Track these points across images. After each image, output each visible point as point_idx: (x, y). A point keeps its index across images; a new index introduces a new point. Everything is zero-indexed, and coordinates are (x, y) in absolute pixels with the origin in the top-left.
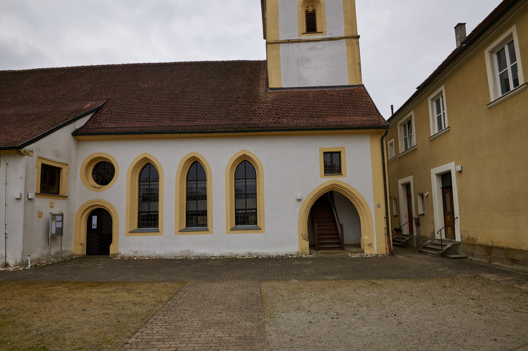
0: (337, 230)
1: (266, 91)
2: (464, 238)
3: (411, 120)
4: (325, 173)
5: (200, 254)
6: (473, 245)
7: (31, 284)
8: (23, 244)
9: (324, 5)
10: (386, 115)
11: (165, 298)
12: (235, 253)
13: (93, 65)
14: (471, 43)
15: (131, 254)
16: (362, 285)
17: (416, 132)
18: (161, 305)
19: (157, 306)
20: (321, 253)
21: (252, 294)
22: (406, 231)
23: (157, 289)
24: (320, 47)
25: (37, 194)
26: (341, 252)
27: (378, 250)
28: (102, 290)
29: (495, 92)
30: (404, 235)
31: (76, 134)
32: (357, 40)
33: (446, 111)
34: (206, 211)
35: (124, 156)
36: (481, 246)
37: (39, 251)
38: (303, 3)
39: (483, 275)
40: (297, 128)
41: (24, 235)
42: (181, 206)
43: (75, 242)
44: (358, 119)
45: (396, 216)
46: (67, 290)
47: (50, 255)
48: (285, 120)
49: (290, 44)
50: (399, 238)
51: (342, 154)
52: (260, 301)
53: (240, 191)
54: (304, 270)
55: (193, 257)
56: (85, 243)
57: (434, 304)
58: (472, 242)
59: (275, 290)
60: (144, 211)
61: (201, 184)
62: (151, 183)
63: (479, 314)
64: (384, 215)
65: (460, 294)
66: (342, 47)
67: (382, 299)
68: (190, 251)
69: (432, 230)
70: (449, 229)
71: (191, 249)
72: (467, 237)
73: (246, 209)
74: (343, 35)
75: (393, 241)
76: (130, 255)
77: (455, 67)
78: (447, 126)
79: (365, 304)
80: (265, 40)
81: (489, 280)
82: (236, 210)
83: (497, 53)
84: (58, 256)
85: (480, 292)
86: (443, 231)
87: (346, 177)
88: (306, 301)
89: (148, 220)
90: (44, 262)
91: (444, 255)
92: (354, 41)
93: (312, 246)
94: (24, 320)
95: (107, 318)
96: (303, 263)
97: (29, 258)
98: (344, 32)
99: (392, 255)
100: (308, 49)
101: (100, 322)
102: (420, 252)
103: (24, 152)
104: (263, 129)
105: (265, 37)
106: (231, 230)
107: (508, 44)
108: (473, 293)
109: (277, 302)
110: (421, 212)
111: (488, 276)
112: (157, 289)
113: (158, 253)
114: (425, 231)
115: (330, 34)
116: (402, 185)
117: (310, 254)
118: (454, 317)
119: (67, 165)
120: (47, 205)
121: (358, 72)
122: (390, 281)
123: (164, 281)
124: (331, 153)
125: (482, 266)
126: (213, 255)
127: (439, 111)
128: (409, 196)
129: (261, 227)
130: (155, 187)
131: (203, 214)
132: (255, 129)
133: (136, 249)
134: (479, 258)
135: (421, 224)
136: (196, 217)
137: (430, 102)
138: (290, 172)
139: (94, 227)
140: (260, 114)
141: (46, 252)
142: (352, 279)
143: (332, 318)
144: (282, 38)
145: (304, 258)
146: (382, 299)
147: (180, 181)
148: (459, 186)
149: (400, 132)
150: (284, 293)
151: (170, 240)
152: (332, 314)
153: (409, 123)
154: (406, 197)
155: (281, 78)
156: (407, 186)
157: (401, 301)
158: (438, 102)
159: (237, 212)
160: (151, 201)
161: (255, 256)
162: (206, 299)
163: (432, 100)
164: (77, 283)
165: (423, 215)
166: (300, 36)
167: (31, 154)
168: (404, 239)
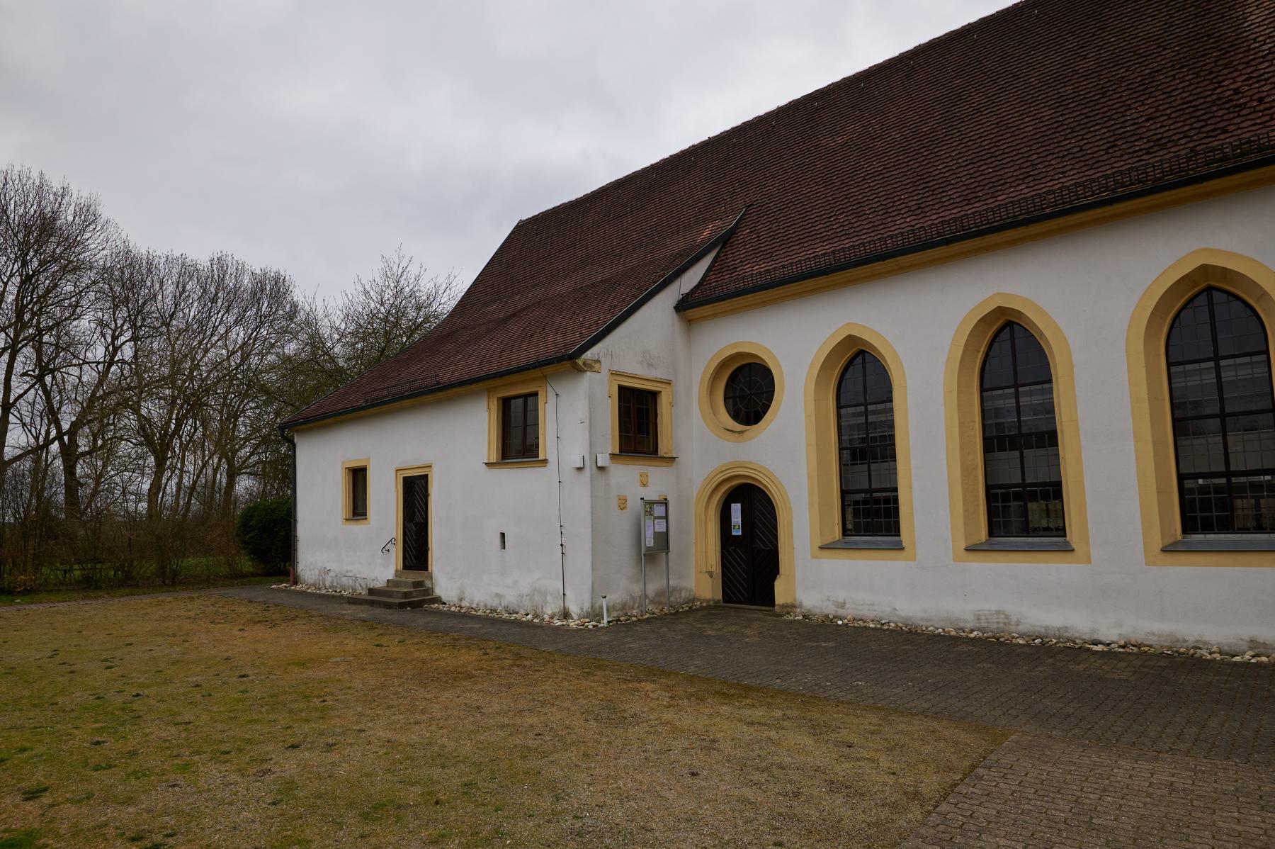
5: (1047, 628)
7: (599, 667)
8: (593, 570)
11: (931, 783)
13: (524, 218)
15: (830, 610)
18: (915, 813)
19: (905, 810)
23: (904, 739)
25: (613, 456)
28: (748, 712)
31: (683, 306)
34: (1058, 485)
35: (796, 340)
37: (624, 588)
41: (593, 550)
42: (966, 472)
43: (697, 570)
46: (665, 697)
47: (646, 597)
55: (1021, 636)
56: (719, 571)
60: (858, 487)
61: (1030, 394)
62: (870, 408)
68: (1007, 617)
76: (826, 611)
82: (1181, 478)
84: (664, 600)
89: (870, 513)
90: (634, 612)
94: (558, 774)
95: (748, 821)
97: (604, 602)
101: (726, 832)
103: (585, 363)
112: (904, 739)
113: (903, 614)
119: (669, 383)
120: (632, 480)
123: (924, 712)
126: (1096, 637)
130: (882, 418)
131: (1045, 496)
133: (841, 596)
136: (1023, 501)
139: (737, 532)
140: (1261, 101)
141: (637, 589)
147: (960, 392)
151: (936, 576)
159: (1189, 484)
160: (875, 458)
164: (691, 679)
167: (597, 366)
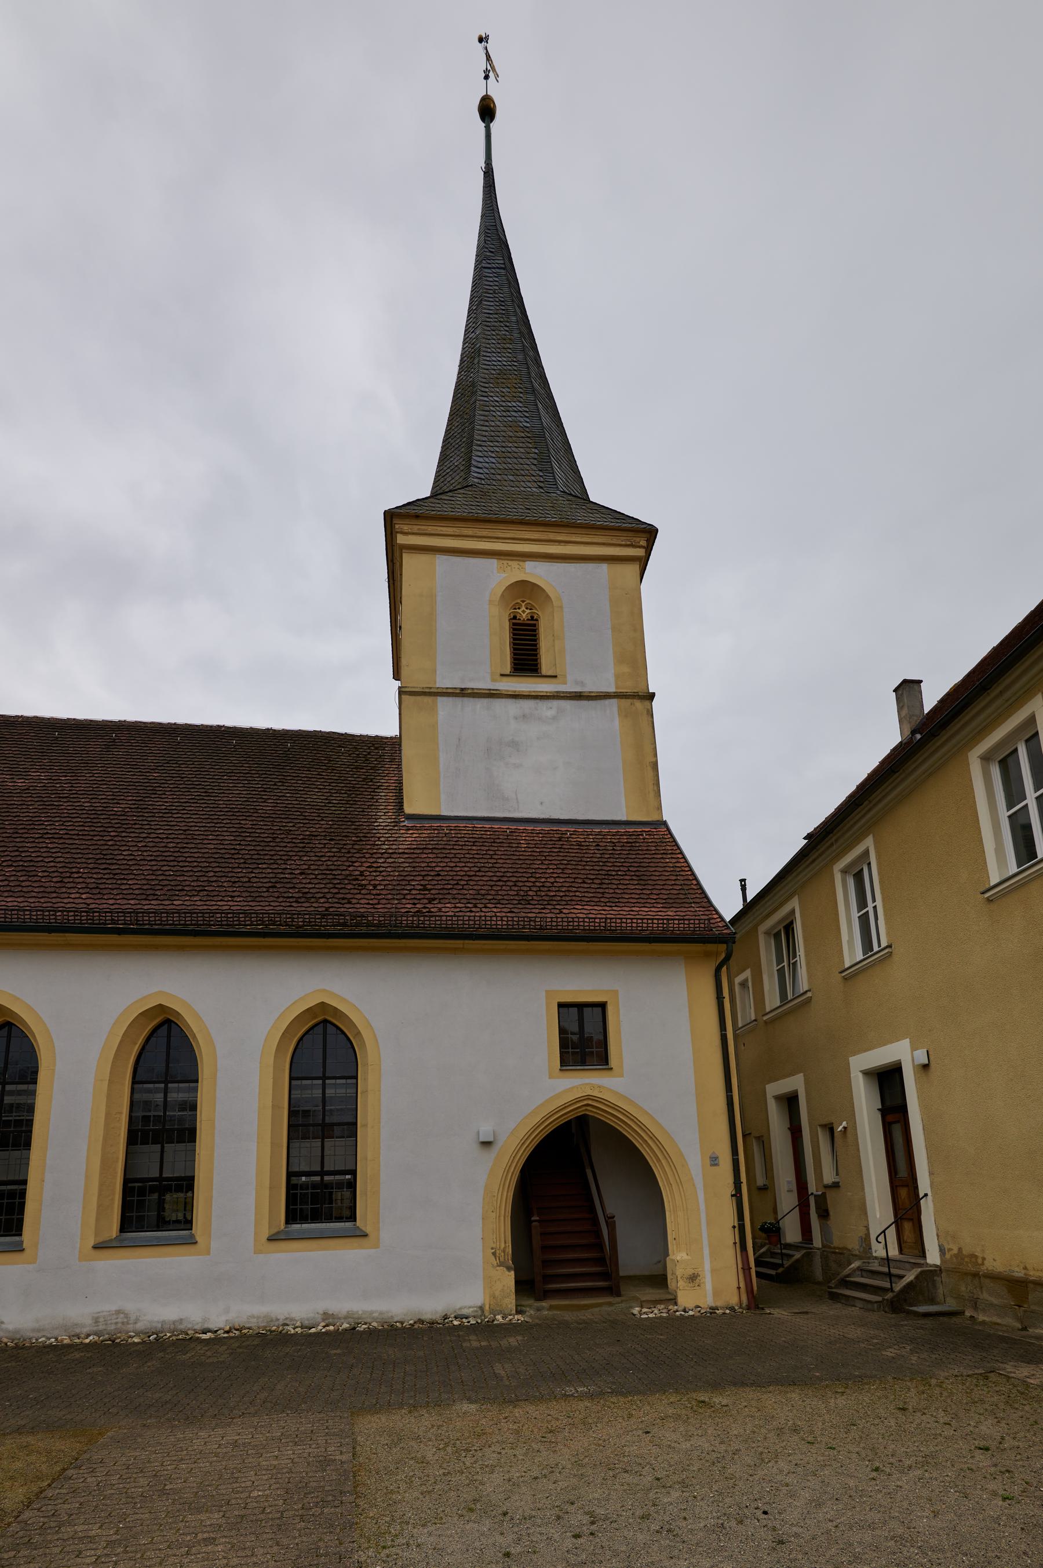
0: (598, 1234)
1: (397, 823)
2: (948, 1256)
3: (792, 923)
4: (564, 1062)
5: (164, 1322)
6: (975, 1275)
9: (561, 607)
10: (728, 905)
12: (281, 1317)
14: (934, 733)
16: (671, 1411)
17: (806, 955)
20: (551, 1308)
21: (325, 1462)
22: (792, 1233)
24: (550, 713)
26: (610, 1304)
27: (716, 1293)
29: (1000, 862)
30: (788, 1246)
32: (647, 703)
33: (879, 903)
36: (995, 1277)
38: (502, 595)
39: (1009, 1368)
40: (481, 932)
42: (106, 1164)
44: (652, 915)
45: (764, 1189)
48: (448, 909)
49: (466, 699)
50: (773, 1255)
51: (610, 1009)
52: (349, 1486)
53: (306, 1113)
54: (498, 1368)
55: (137, 1334)
57: (877, 1469)
58: (971, 1268)
59: (400, 1441)
61: (178, 1090)
63: (1004, 1499)
64: (730, 1189)
65: (948, 1432)
66: (607, 718)
67: (728, 1458)
68: (126, 1316)
69: (862, 1233)
70: (907, 1226)
71: (130, 1307)
72: (955, 1251)
73: (322, 1173)
74: (612, 689)
75: (758, 1263)
77: (899, 789)
78: (884, 944)
79: (676, 1478)
80: (398, 683)
81: (1027, 1385)
82: (290, 1175)
83: (1000, 762)
85: (1003, 1424)
86: (892, 1233)
87: (622, 1076)
88: (497, 1478)
91: (899, 1304)
92: (638, 704)
93: (525, 1286)
96: (494, 1344)
98: (612, 680)
99: (757, 1307)
100: (516, 718)
102: (834, 1297)
104: (383, 930)
105: (397, 676)
106: (270, 1240)
107: (1027, 741)
108: (983, 1428)
109: (403, 1486)
110: (829, 1177)
111: (1023, 1371)
113: (11, 1327)
114: (845, 1237)
115: (577, 683)
116: (778, 1098)
117: (518, 1312)
118: (936, 1514)
121: (651, 787)
122: (750, 1394)
123: (19, 1430)
124: (581, 1006)
125: (1003, 1339)
126: (206, 1326)
127: (862, 903)
128: (795, 1132)
129: (368, 1229)
131: (179, 1189)
132: (357, 930)
134: (994, 1314)
135: (831, 1213)
136: (155, 1202)
137: (838, 877)
138: (458, 1058)
142: (639, 1393)
143: (577, 1536)
144: (444, 681)
145: (500, 1325)
146: (728, 1458)
148: (924, 1107)
149: (766, 952)
150: (430, 1453)
152: (578, 1519)
153: (789, 928)
154: (789, 1133)
155: (441, 788)
156: (790, 1101)
157: (782, 1464)
158: (859, 877)
159: (294, 1180)
161: (346, 1326)
162: (163, 1492)
163: (845, 871)
165: (836, 1185)
166: (493, 680)
168: (790, 1256)
